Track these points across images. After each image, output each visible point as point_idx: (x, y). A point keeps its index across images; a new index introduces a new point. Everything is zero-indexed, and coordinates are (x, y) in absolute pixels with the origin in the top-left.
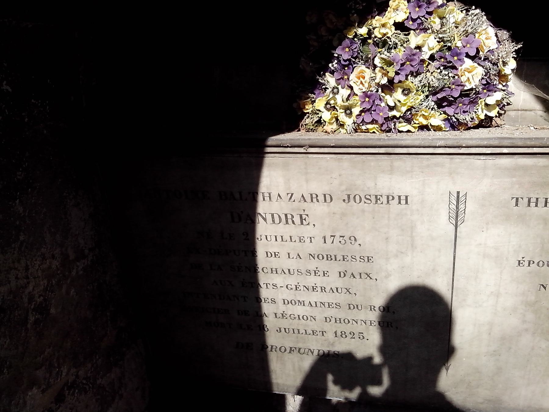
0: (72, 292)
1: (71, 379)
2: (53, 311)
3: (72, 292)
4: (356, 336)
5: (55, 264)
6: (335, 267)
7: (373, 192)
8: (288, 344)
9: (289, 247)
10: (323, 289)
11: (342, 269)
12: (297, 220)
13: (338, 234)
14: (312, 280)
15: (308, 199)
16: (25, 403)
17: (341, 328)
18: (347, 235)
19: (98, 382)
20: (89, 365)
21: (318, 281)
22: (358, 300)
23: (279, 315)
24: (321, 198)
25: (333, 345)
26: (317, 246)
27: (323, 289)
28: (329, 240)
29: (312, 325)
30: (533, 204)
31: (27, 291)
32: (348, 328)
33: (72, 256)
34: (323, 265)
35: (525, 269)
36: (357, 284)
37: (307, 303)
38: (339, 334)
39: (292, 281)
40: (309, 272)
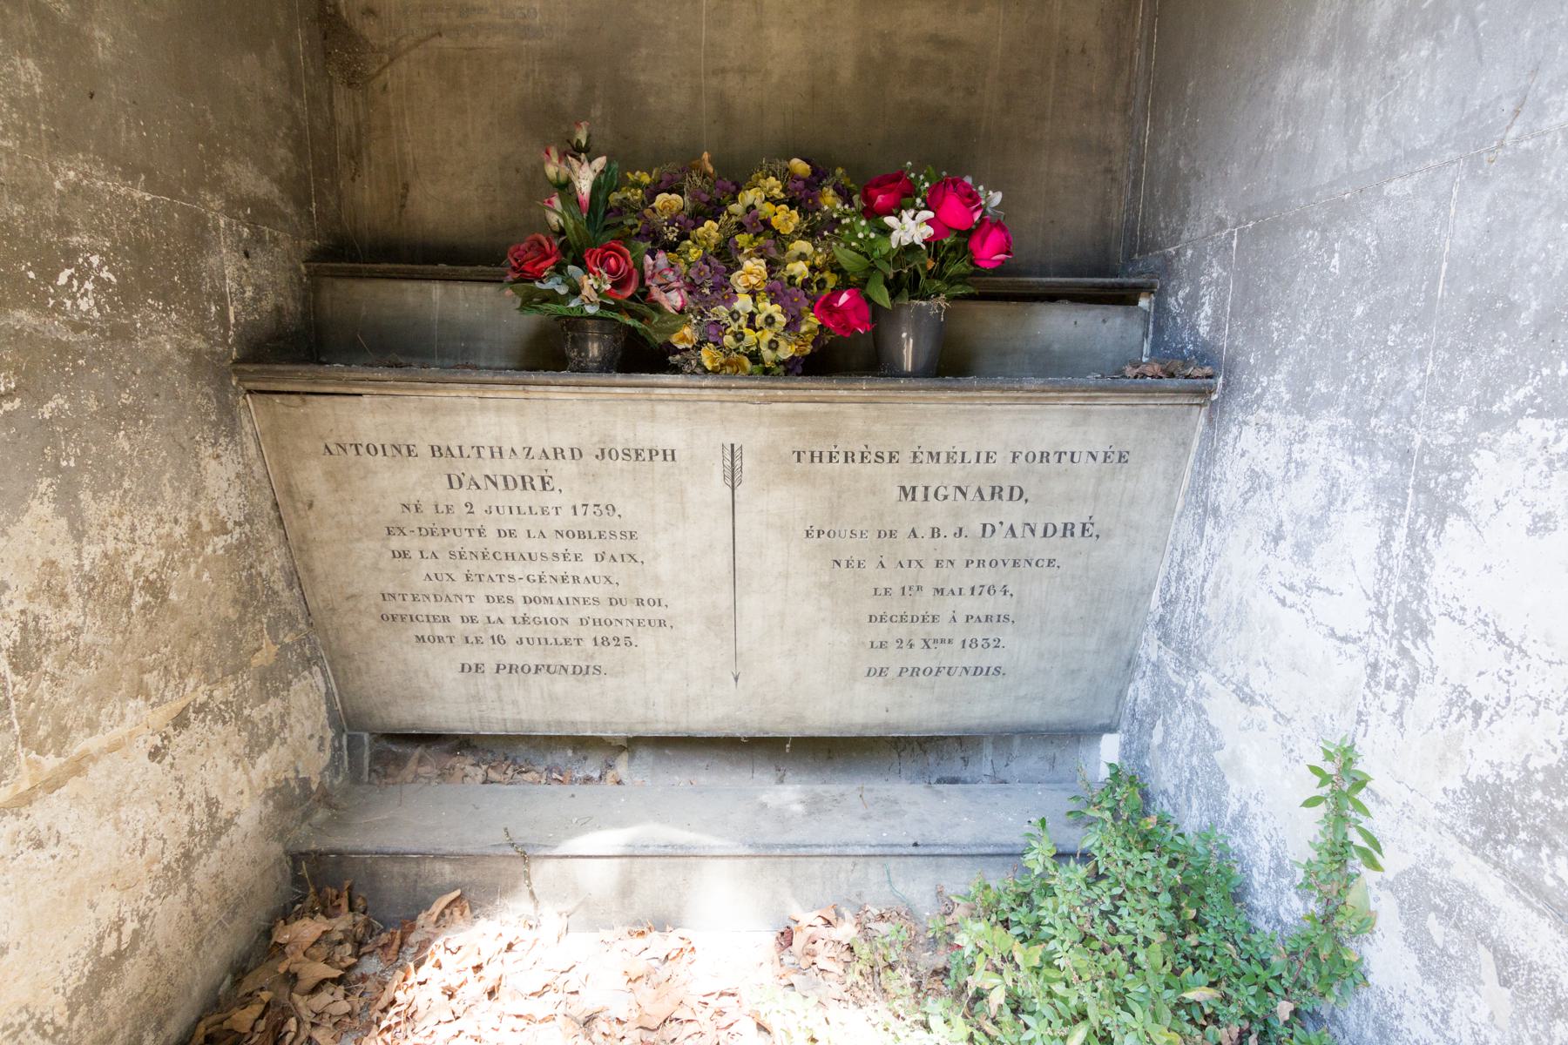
0: (206, 576)
1: (202, 698)
2: (173, 596)
3: (206, 576)
4: (622, 642)
5: (180, 531)
6: (588, 548)
7: (632, 446)
8: (532, 661)
9: (528, 522)
10: (576, 579)
11: (599, 551)
12: (538, 483)
13: (591, 503)
14: (560, 567)
15: (551, 454)
16: (123, 716)
17: (602, 632)
18: (603, 503)
19: (246, 712)
20: (232, 686)
21: (569, 568)
22: (620, 592)
23: (519, 620)
24: (568, 454)
25: (592, 657)
26: (564, 520)
27: (576, 579)
28: (580, 511)
29: (563, 631)
30: (817, 460)
31: (132, 560)
32: (610, 632)
33: (206, 527)
34: (575, 545)
35: (815, 540)
36: (619, 570)
37: (555, 600)
38: (599, 641)
39: (534, 569)
40: (556, 556)
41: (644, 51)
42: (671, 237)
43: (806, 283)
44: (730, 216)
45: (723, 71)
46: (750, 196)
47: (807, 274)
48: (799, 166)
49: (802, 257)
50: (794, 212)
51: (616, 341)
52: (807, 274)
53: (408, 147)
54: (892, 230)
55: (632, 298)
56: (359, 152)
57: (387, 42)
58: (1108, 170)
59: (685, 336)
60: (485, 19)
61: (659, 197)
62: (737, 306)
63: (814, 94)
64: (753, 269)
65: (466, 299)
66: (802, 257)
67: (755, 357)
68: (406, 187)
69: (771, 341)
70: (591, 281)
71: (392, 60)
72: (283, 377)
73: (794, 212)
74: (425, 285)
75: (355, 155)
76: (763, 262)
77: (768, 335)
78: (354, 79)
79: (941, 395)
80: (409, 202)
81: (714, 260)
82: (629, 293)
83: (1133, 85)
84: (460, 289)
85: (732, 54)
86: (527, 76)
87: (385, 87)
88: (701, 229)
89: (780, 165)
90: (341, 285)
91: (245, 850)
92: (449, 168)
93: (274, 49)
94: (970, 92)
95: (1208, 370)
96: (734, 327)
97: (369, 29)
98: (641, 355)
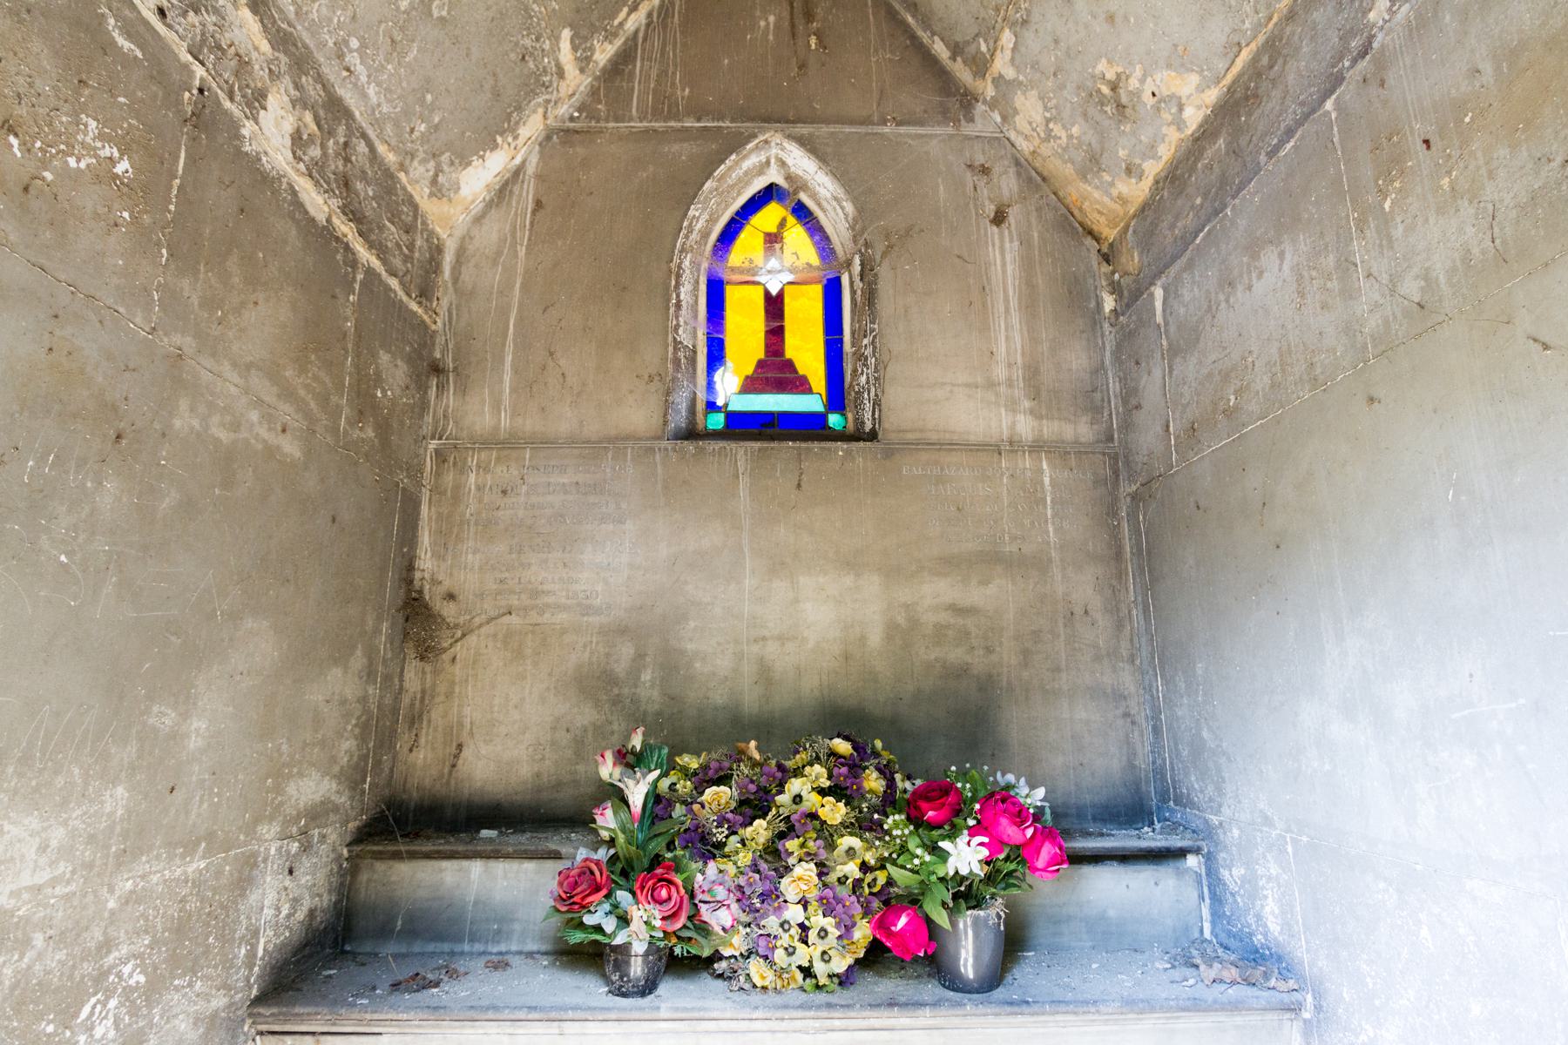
41: (692, 624)
42: (720, 837)
43: (858, 883)
45: (764, 639)
46: (795, 786)
47: (858, 875)
48: (842, 746)
50: (841, 805)
51: (660, 959)
52: (858, 875)
53: (467, 711)
55: (685, 926)
56: (420, 716)
57: (461, 620)
58: (1126, 715)
59: (737, 944)
60: (550, 600)
61: (708, 791)
63: (847, 657)
64: (801, 879)
65: (505, 877)
66: (851, 852)
67: (807, 972)
68: (460, 747)
69: (824, 953)
70: (641, 912)
71: (464, 635)
72: (300, 1018)
73: (841, 805)
74: (465, 863)
75: (415, 720)
76: (812, 865)
77: (821, 946)
78: (426, 652)
79: (1011, 1019)
80: (460, 762)
81: (763, 866)
82: (679, 925)
83: (1136, 640)
84: (500, 867)
85: (771, 625)
86: (585, 646)
87: (454, 659)
88: (749, 829)
90: (380, 866)
91: (315, 339)
92: (502, 729)
93: (359, 653)
94: (989, 650)
95: (1292, 984)
96: (785, 940)
97: (448, 611)
98: (683, 961)
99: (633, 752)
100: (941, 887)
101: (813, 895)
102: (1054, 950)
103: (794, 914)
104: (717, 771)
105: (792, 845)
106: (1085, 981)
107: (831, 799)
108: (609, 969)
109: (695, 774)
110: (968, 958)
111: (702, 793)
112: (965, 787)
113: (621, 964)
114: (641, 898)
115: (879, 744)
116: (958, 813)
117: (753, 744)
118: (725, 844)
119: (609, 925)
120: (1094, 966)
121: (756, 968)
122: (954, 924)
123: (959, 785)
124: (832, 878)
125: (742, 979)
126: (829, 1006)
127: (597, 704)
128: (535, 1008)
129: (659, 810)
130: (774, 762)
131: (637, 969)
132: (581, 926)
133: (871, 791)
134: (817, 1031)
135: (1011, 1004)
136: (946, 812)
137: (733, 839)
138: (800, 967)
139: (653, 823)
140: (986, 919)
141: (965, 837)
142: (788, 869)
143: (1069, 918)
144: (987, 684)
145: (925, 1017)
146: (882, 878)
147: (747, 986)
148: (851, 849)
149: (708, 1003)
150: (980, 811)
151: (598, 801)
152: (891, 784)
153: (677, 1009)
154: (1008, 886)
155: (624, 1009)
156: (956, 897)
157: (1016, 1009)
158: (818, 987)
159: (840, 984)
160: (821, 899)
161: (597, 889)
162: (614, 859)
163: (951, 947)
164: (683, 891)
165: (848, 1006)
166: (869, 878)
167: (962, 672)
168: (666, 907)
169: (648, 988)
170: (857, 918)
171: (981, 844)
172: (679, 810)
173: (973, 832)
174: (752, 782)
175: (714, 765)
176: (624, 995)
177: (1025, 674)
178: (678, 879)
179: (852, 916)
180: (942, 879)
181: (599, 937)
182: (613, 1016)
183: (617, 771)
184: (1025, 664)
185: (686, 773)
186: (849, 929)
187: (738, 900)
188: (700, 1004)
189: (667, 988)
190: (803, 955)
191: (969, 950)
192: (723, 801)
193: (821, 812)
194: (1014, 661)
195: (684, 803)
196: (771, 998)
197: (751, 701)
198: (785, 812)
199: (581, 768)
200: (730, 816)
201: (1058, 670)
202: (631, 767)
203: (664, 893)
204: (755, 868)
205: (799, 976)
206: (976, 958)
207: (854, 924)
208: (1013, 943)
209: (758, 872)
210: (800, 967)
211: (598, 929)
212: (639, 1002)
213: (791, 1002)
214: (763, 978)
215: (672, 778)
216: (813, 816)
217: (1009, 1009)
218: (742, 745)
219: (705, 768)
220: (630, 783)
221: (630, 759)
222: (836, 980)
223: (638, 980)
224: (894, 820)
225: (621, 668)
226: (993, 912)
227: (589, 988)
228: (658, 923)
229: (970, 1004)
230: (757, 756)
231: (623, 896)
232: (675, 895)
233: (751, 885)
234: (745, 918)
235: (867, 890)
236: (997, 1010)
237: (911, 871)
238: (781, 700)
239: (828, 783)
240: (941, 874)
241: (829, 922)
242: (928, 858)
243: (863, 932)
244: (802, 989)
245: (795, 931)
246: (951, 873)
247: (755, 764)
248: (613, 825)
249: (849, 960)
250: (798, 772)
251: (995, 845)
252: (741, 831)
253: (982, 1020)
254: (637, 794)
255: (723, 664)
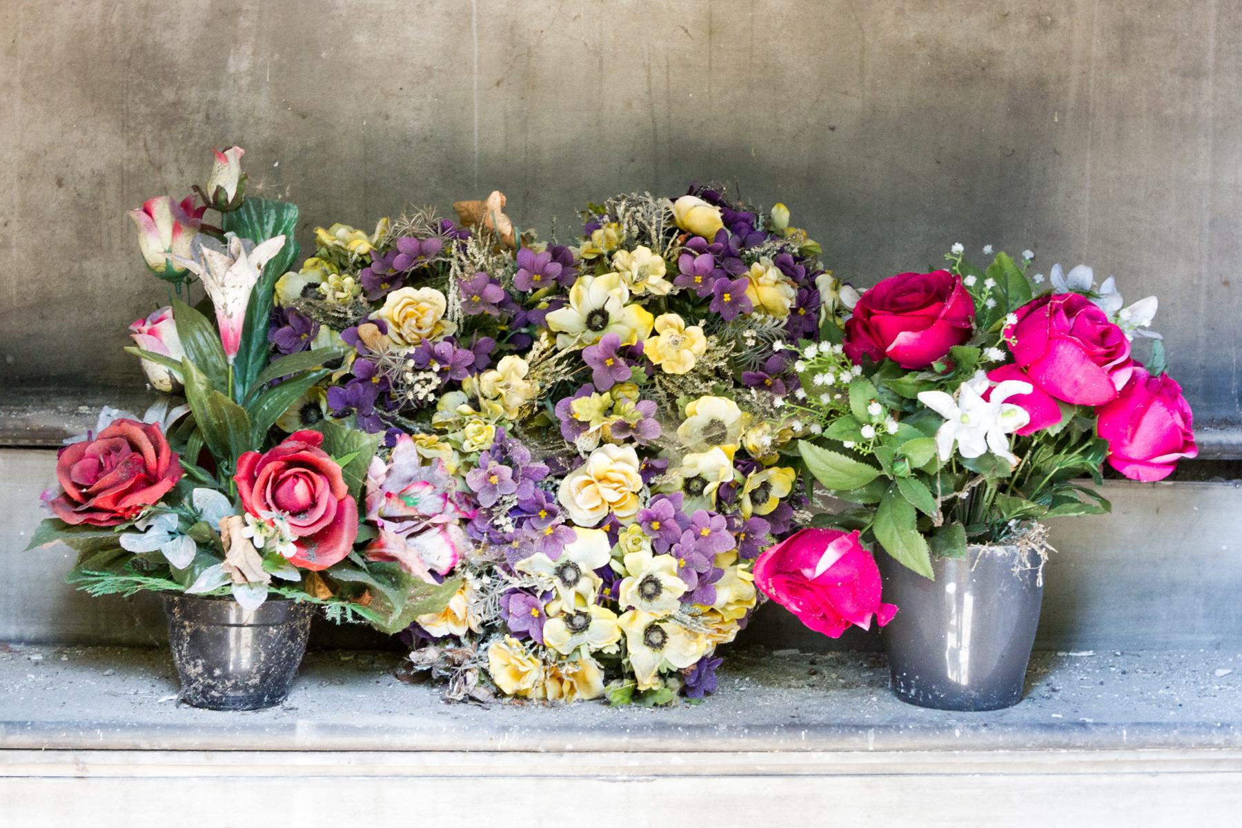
42: (423, 392)
44: (553, 336)
46: (590, 291)
47: (730, 474)
48: (701, 215)
49: (715, 434)
50: (697, 331)
51: (293, 636)
52: (730, 474)
54: (939, 418)
55: (347, 563)
62: (572, 551)
63: (712, 28)
64: (606, 475)
66: (715, 434)
67: (614, 667)
69: (652, 628)
70: (251, 530)
73: (697, 331)
76: (630, 451)
81: (521, 451)
82: (336, 556)
88: (489, 377)
89: (654, 210)
94: (1042, 23)
96: (567, 601)
98: (346, 641)
99: (218, 203)
100: (921, 488)
101: (630, 511)
102: (1135, 648)
103: (589, 549)
104: (412, 258)
105: (585, 406)
106: (1201, 694)
107: (675, 318)
108: (181, 652)
109: (363, 263)
110: (960, 652)
111: (379, 303)
112: (983, 289)
113: (209, 645)
114: (252, 499)
115: (781, 214)
116: (965, 336)
117: (496, 199)
118: (433, 406)
119: (181, 554)
120: (1220, 672)
121: (503, 658)
122: (938, 567)
123: (970, 281)
124: (674, 479)
125: (472, 678)
126: (661, 727)
127: (126, 126)
128: (22, 725)
129: (280, 336)
130: (542, 247)
131: (243, 653)
132: (121, 560)
133: (763, 308)
134: (633, 776)
135: (1049, 726)
136: (938, 332)
137: (450, 398)
138: (598, 655)
139: (267, 363)
140: (1008, 563)
141: (980, 381)
142: (576, 459)
143: (1173, 587)
144: (1033, 100)
145: (865, 752)
146: (782, 481)
147: (482, 693)
148: (714, 423)
149: (396, 720)
150: (1015, 330)
151: (145, 310)
152: (808, 296)
153: (332, 729)
154: (1057, 502)
155: (218, 729)
156: (947, 508)
157: (1059, 737)
158: (637, 696)
159: (683, 693)
160: (649, 519)
161: (150, 480)
162: (183, 429)
163: (925, 624)
164: (342, 488)
165: (701, 728)
166: (754, 480)
167: (976, 70)
168: (303, 520)
169: (267, 692)
170: (725, 563)
171: (1014, 400)
172: (327, 340)
173: (997, 372)
174: (494, 281)
175: (405, 244)
176: (216, 705)
177: (1121, 80)
178: (334, 465)
179: (713, 559)
180: (919, 474)
181: (164, 584)
182: (195, 741)
183: (184, 242)
184: (1121, 59)
185: (340, 261)
186: (707, 580)
187: (465, 521)
188: (383, 720)
189: (315, 706)
190: (605, 630)
191: (962, 630)
192: (428, 321)
193: (653, 350)
194: (1098, 50)
195: (339, 324)
196: (534, 714)
197: (487, 124)
198: (567, 345)
199: (95, 268)
200: (444, 348)
201: (1194, 73)
202: (218, 234)
203: (301, 491)
204: (502, 454)
205: (595, 674)
206: (980, 640)
207: (719, 574)
208: (1052, 630)
209: (510, 462)
210: (598, 655)
211: (159, 566)
212: (251, 717)
213: (580, 720)
214: (518, 675)
215: (310, 272)
216: (632, 354)
217: (1043, 737)
218: (471, 205)
219: (386, 251)
220: (216, 258)
221: (212, 218)
222: (675, 683)
223: (248, 675)
224: (822, 362)
225: (178, 39)
226: (1026, 547)
227: (140, 698)
228: (289, 551)
229: (960, 726)
230: (505, 226)
231: (206, 499)
232: (324, 495)
233: (493, 488)
234: (477, 557)
235: (748, 507)
236: (1019, 738)
237: (854, 454)
238: (556, 128)
239: (666, 288)
240: (920, 461)
241: (664, 567)
242: (893, 427)
243: (738, 589)
244: (602, 699)
245: (590, 585)
246: (945, 456)
247: (497, 243)
248: (177, 354)
249: (703, 647)
250: (599, 264)
251: (1044, 402)
252: (469, 382)
253: (985, 757)
254: (233, 282)
255: (422, 38)
